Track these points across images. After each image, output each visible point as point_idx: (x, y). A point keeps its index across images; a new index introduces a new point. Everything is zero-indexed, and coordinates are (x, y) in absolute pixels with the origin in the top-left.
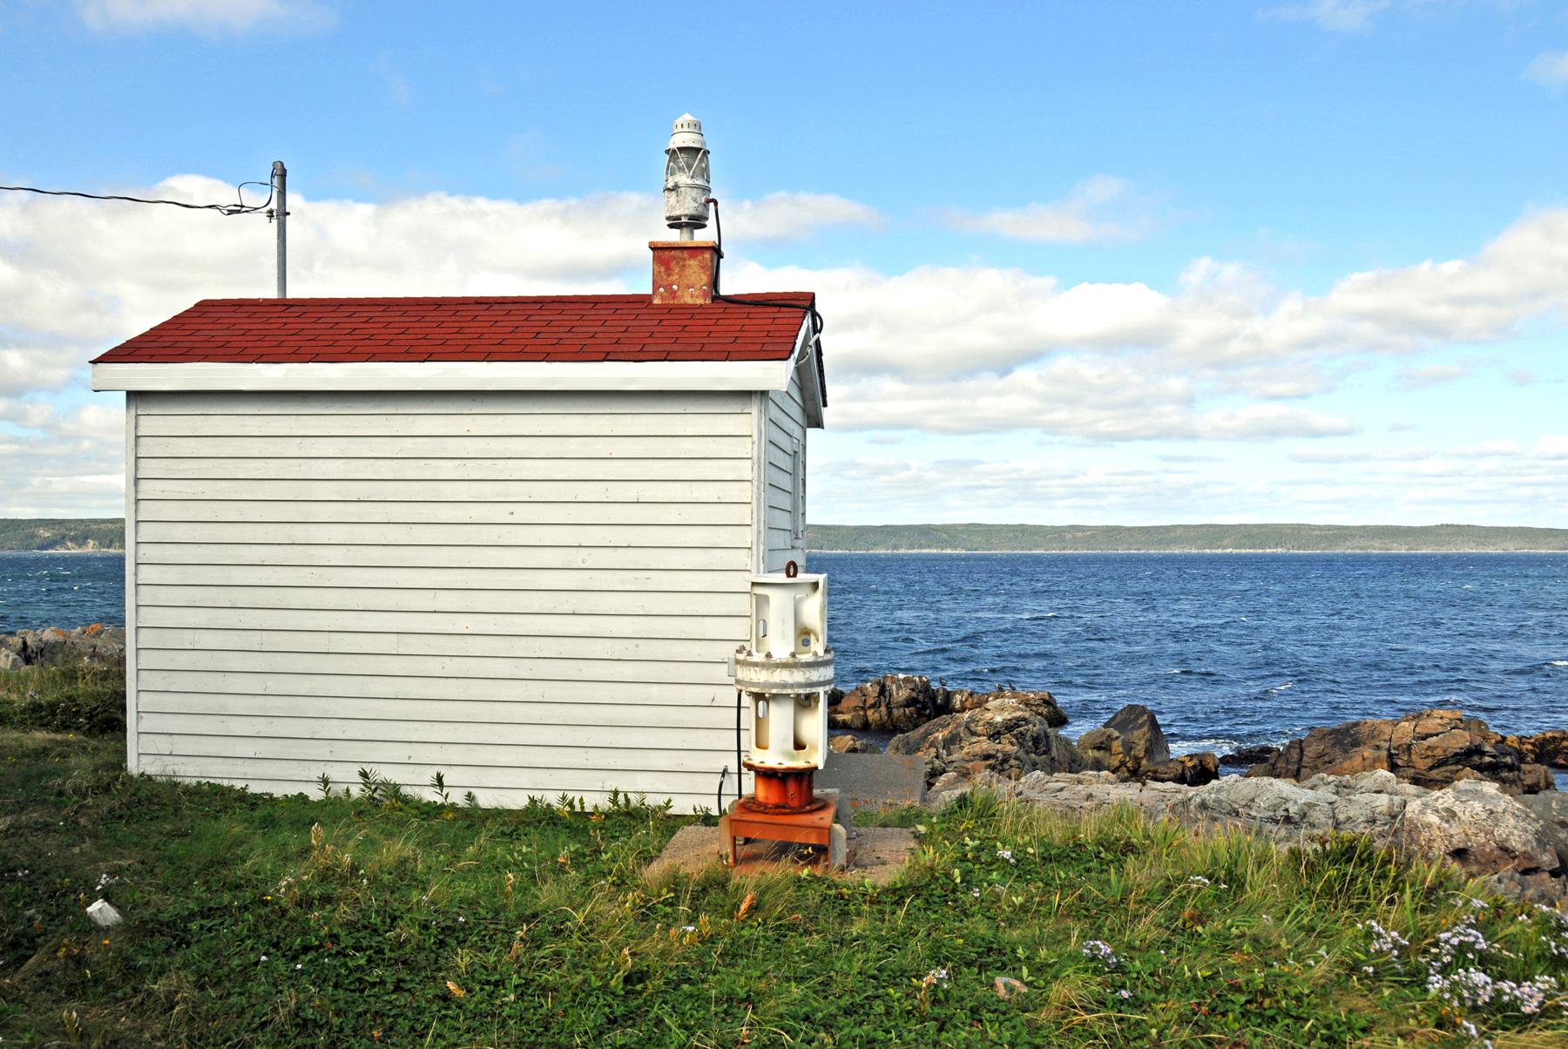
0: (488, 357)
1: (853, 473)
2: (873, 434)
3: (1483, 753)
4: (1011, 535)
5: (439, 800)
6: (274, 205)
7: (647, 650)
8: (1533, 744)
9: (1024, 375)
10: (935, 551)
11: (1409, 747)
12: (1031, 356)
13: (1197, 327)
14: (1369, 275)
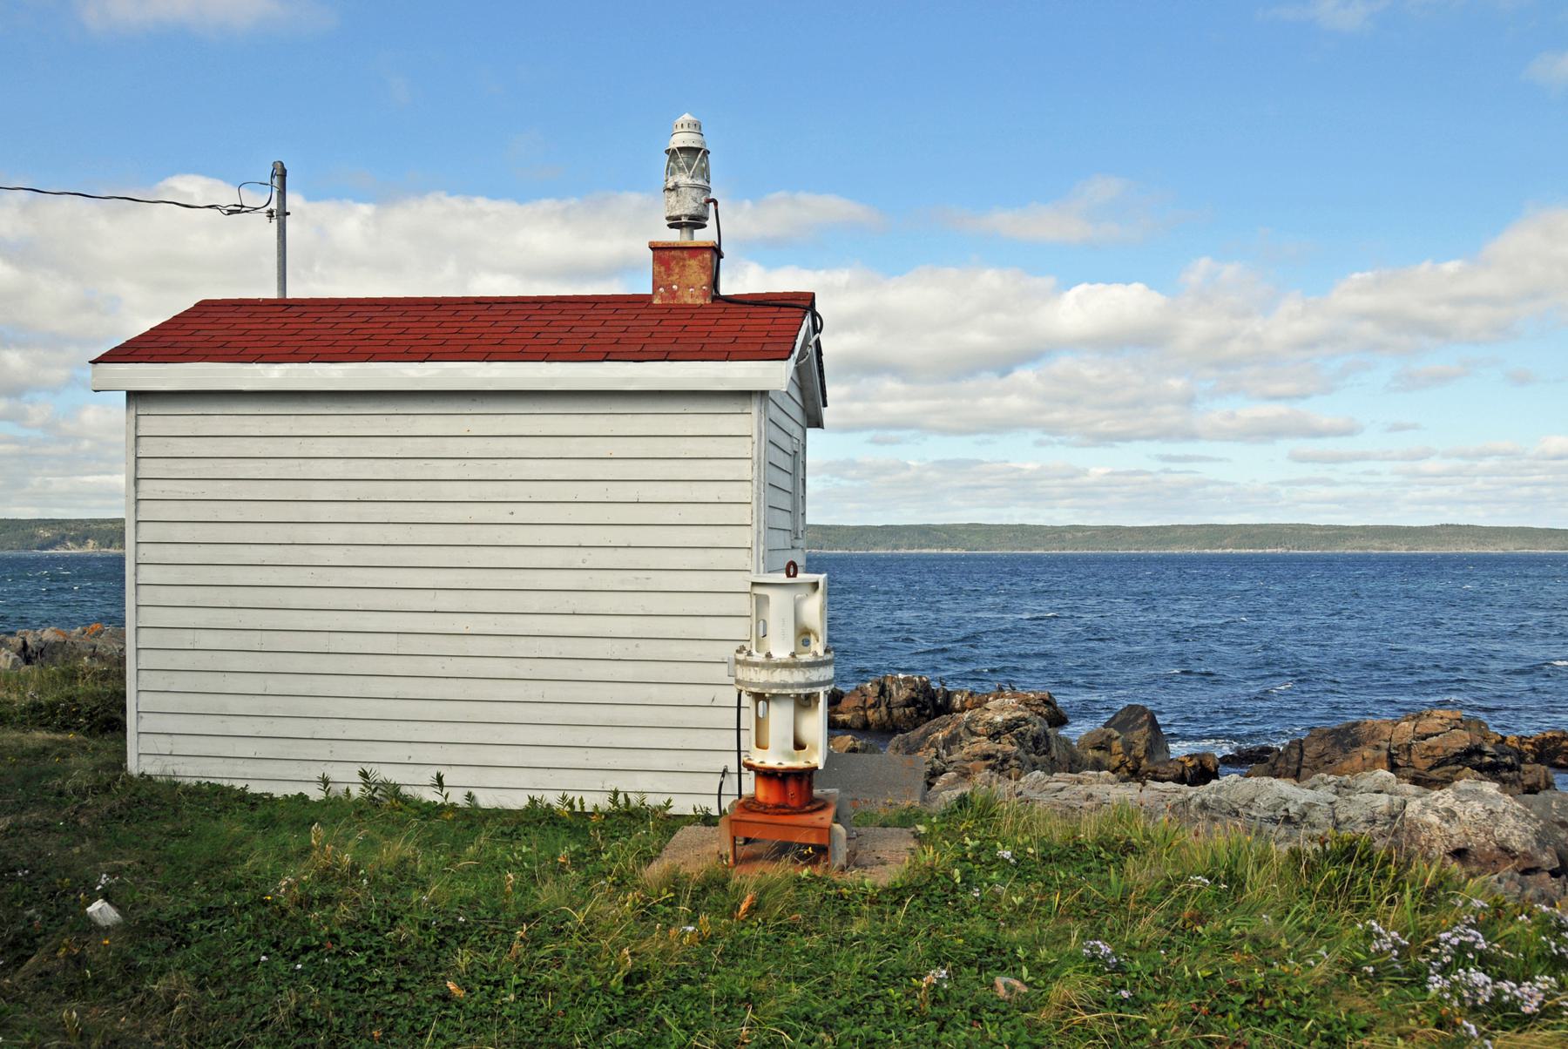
0: (488, 357)
3: (1483, 753)
6: (274, 206)
7: (648, 650)
8: (1533, 744)
10: (935, 551)
11: (1409, 747)
12: (1031, 356)
13: (1197, 327)
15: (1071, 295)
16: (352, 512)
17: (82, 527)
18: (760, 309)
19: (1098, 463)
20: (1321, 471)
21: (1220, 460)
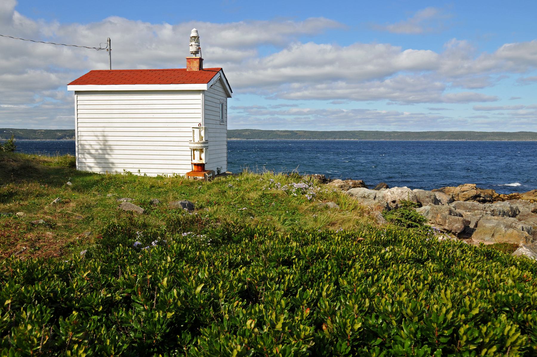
0: (148, 83)
1: (324, 113)
2: (331, 101)
3: (480, 197)
4: (373, 134)
5: (139, 175)
6: (108, 48)
7: (180, 144)
8: (508, 197)
9: (388, 81)
10: (348, 140)
11: (458, 194)
12: (389, 74)
13: (448, 64)
14: (512, 44)
15: (406, 52)
16: (121, 116)
17: (71, 132)
18: (209, 72)
19: (406, 111)
20: (484, 113)
21: (448, 109)
